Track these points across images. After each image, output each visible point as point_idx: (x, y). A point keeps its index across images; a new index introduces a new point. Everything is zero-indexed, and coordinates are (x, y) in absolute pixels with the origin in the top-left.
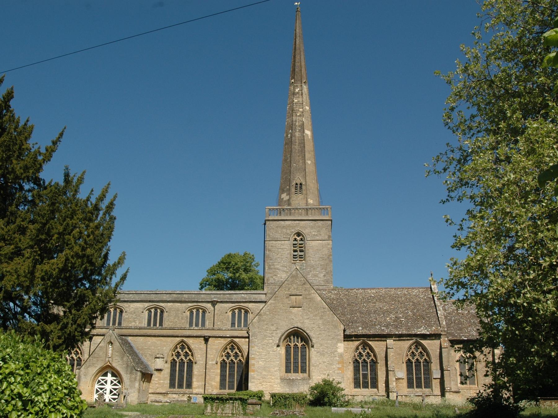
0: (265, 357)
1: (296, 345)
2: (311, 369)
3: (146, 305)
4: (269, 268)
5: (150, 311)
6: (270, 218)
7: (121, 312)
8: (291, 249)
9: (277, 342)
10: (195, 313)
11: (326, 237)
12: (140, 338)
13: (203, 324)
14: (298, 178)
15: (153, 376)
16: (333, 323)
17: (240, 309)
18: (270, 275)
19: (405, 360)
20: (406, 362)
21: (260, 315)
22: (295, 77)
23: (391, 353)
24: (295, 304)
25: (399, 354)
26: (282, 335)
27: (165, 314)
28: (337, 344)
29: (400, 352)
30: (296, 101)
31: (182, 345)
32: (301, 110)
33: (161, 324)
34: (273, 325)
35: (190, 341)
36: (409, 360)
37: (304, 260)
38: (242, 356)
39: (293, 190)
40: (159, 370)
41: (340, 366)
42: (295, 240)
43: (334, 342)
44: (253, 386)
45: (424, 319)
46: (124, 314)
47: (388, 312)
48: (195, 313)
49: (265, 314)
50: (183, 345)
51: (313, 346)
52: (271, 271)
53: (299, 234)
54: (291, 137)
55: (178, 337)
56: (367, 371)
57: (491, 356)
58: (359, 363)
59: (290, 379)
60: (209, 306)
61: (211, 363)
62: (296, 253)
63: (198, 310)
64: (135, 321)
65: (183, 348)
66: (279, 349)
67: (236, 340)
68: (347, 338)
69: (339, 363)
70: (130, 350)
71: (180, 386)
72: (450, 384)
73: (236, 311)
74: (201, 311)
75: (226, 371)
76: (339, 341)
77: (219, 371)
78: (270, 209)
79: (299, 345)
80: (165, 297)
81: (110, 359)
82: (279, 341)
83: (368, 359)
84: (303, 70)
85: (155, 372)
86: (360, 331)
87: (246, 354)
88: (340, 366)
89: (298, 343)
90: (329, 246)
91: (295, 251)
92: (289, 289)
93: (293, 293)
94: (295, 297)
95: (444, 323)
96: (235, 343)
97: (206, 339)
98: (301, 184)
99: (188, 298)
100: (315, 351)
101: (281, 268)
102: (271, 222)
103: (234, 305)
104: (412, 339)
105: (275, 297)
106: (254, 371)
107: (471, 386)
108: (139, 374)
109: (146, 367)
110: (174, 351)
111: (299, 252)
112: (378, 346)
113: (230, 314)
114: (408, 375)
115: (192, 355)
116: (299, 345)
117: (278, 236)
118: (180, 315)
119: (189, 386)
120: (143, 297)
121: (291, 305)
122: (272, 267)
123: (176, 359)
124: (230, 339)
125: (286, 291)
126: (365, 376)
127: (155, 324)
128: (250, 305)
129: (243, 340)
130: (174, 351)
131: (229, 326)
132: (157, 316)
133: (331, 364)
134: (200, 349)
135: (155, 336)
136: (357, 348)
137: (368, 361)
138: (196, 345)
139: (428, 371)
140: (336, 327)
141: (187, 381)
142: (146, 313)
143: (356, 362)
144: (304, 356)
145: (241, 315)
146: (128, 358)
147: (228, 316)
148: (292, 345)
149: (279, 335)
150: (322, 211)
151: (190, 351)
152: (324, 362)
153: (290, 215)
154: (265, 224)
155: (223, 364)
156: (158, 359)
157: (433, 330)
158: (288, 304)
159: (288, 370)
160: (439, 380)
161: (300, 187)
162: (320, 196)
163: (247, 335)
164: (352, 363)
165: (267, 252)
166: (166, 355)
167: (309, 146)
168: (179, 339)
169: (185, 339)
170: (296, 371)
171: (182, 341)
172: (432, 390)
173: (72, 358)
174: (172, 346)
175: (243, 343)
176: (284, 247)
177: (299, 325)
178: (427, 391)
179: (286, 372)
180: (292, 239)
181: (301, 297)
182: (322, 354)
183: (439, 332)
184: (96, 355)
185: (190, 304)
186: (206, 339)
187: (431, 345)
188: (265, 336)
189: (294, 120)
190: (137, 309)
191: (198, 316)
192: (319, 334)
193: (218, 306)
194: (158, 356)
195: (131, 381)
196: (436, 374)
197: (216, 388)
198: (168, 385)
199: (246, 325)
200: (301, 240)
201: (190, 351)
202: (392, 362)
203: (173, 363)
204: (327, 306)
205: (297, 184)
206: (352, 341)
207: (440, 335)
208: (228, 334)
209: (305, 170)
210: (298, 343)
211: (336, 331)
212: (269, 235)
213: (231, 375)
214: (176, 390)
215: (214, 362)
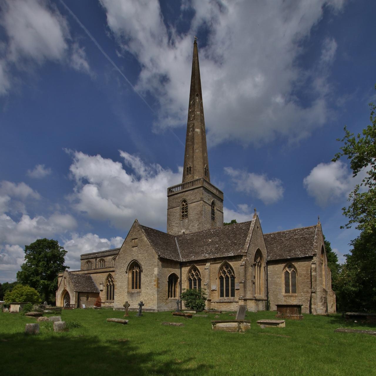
0: (121, 280)
1: (136, 271)
8: (180, 211)
11: (200, 199)
15: (100, 294)
34: (124, 260)
40: (102, 291)
57: (106, 258)
59: (131, 293)
85: (100, 292)
93: (134, 238)
100: (143, 274)
105: (126, 242)
107: (293, 294)
121: (132, 246)
133: (151, 282)
136: (221, 268)
152: (147, 281)
158: (132, 245)
166: (104, 282)
168: (108, 273)
169: (111, 273)
181: (137, 240)
182: (147, 276)
188: (121, 267)
194: (101, 283)
205: (188, 168)
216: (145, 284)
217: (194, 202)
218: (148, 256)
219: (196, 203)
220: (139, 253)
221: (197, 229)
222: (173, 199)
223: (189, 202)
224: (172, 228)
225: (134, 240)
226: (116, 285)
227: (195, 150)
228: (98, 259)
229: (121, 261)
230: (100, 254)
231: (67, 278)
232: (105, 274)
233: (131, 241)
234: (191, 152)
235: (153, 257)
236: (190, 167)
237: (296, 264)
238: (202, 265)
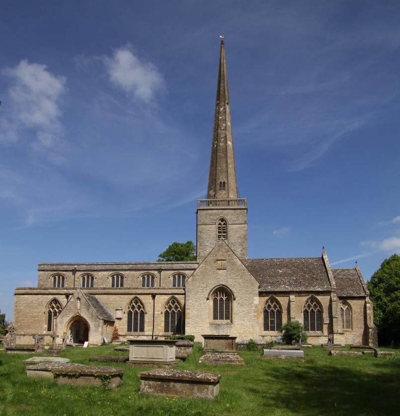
1: (221, 298)
2: (233, 316)
4: (201, 245)
5: (114, 278)
6: (201, 208)
7: (93, 278)
9: (207, 296)
10: (146, 278)
11: (243, 222)
12: (104, 295)
13: (153, 285)
14: (222, 179)
15: (115, 323)
16: (251, 282)
17: (179, 275)
18: (201, 250)
19: (303, 310)
20: (304, 312)
21: (194, 276)
22: (220, 98)
23: (293, 305)
24: (221, 267)
25: (298, 306)
26: (211, 291)
27: (125, 279)
28: (253, 297)
29: (300, 304)
30: (220, 118)
31: (136, 300)
32: (224, 125)
34: (203, 283)
35: (141, 297)
36: (306, 310)
37: (227, 239)
38: (181, 308)
39: (218, 187)
40: (119, 319)
41: (256, 314)
42: (220, 224)
44: (189, 331)
46: (94, 280)
48: (146, 278)
50: (137, 300)
51: (234, 299)
52: (202, 247)
53: (222, 220)
54: (217, 146)
55: (132, 294)
56: (274, 318)
58: (268, 312)
60: (156, 273)
61: (157, 313)
62: (220, 234)
63: (148, 277)
65: (136, 303)
66: (208, 301)
67: (176, 296)
68: (261, 294)
69: (255, 312)
70: (97, 304)
71: (136, 330)
72: (337, 328)
73: (177, 276)
74: (150, 276)
75: (169, 319)
76: (255, 295)
77: (163, 319)
78: (201, 201)
79: (224, 298)
80: (124, 267)
81: (79, 311)
83: (275, 309)
84: (225, 65)
85: (116, 321)
86: (269, 288)
87: (183, 305)
88: (256, 314)
89: (223, 300)
90: (245, 229)
91: (219, 232)
92: (216, 256)
93: (220, 258)
94: (220, 262)
95: (334, 283)
96: (175, 298)
97: (154, 296)
98: (224, 183)
101: (209, 245)
102: (202, 211)
103: (174, 272)
104: (308, 295)
106: (189, 318)
107: (348, 329)
108: (102, 321)
109: (110, 316)
110: (130, 305)
111: (223, 232)
112: (283, 300)
113: (172, 278)
114: (304, 321)
115: (144, 308)
116: (224, 298)
117: (208, 221)
118: (135, 280)
119: (142, 330)
121: (218, 268)
123: (132, 310)
124: (171, 296)
125: (213, 257)
126: (272, 322)
127: (117, 286)
128: (187, 272)
129: (181, 296)
130: (130, 305)
131: (171, 286)
132: (118, 279)
134: (149, 303)
135: (115, 294)
136: (267, 302)
137: (275, 311)
138: (147, 300)
139: (321, 318)
140: (252, 284)
141: (140, 326)
142: (111, 279)
143: (266, 312)
144: (228, 307)
145: (180, 279)
146: (93, 310)
147: (171, 280)
148: (219, 298)
149: (209, 291)
150: (239, 201)
152: (244, 311)
153: (216, 205)
154: (197, 213)
155: (167, 314)
156: (118, 311)
157: (325, 288)
159: (215, 318)
160: (327, 325)
161: (223, 185)
162: (238, 193)
163: (183, 292)
164: (263, 312)
165: (199, 233)
166: (124, 308)
167: (230, 154)
168: (133, 296)
170: (222, 318)
171: (136, 297)
172: (323, 332)
173: (55, 311)
174: (128, 301)
175: (180, 298)
176: (211, 229)
177: (224, 283)
178: (319, 333)
179: (214, 319)
180: (217, 223)
181: (225, 262)
182: (242, 305)
183: (331, 290)
184: (68, 308)
185: (142, 272)
186: (154, 296)
187: (324, 300)
189: (219, 133)
190: (104, 275)
191: (148, 279)
192: (240, 290)
193: (163, 273)
194: (118, 308)
195: (95, 327)
196: (326, 320)
197: (162, 331)
198: (127, 329)
199: (184, 285)
200: (224, 224)
202: (294, 312)
203: (130, 313)
204: (246, 269)
205: (221, 183)
206: (264, 296)
207: (331, 291)
208: (170, 291)
209: (227, 172)
210: (223, 300)
211: (253, 287)
212: (200, 221)
213: (173, 322)
214: (133, 332)
215: (160, 313)
216: (240, 314)
217: (237, 224)
219: (239, 225)
220: (229, 277)
221: (240, 254)
222: (206, 215)
223: (229, 222)
224: (204, 248)
225: (219, 262)
227: (229, 164)
228: (78, 274)
229: (198, 284)
230: (85, 266)
231: (83, 300)
232: (126, 296)
233: (215, 262)
234: (224, 165)
235: (252, 284)
236: (224, 183)
237: (352, 302)
238: (282, 296)
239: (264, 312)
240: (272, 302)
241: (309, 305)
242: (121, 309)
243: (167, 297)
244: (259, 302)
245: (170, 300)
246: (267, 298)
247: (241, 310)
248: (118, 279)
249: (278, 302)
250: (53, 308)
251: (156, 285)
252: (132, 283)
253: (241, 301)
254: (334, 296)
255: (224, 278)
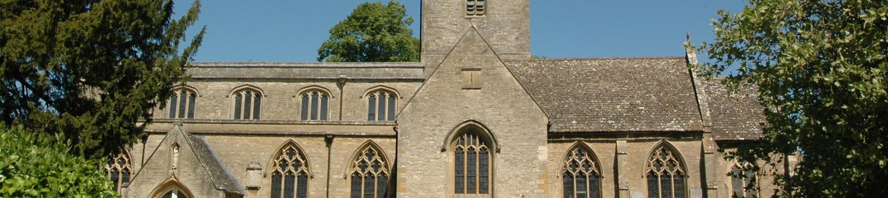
2: (495, 187)
3: (233, 85)
4: (429, 27)
5: (240, 96)
7: (193, 96)
9: (442, 144)
12: (223, 137)
13: (324, 116)
16: (532, 114)
17: (382, 92)
18: (430, 38)
19: (646, 172)
20: (648, 176)
21: (415, 101)
24: (470, 83)
26: (450, 133)
29: (638, 160)
31: (291, 148)
33: (256, 116)
34: (434, 117)
35: (302, 143)
36: (652, 172)
38: (386, 166)
40: (254, 189)
41: (542, 182)
43: (533, 143)
45: (676, 107)
46: (197, 100)
47: (619, 96)
49: (423, 99)
50: (292, 149)
51: (498, 151)
52: (432, 31)
55: (283, 135)
58: (572, 177)
60: (333, 86)
61: (336, 177)
63: (315, 94)
64: (214, 111)
65: (291, 154)
66: (444, 154)
67: (377, 141)
68: (554, 137)
70: (207, 156)
73: (377, 95)
76: (540, 143)
79: (477, 148)
80: (263, 73)
82: (445, 143)
85: (248, 192)
86: (574, 126)
87: (393, 163)
88: (542, 182)
92: (460, 60)
93: (467, 66)
94: (469, 72)
96: (374, 145)
97: (329, 140)
99: (300, 75)
100: (502, 158)
103: (372, 85)
106: (404, 190)
113: (366, 99)
115: (306, 165)
116: (477, 148)
118: (287, 101)
120: (227, 73)
121: (464, 85)
122: (434, 24)
123: (280, 171)
124: (366, 140)
125: (455, 63)
127: (247, 116)
128: (399, 86)
129: (388, 140)
130: (278, 159)
131: (365, 119)
132: (250, 103)
133: (528, 180)
134: (320, 155)
135: (247, 135)
136: (569, 154)
137: (587, 174)
138: (313, 148)
140: (535, 120)
142: (233, 98)
143: (567, 175)
144: (484, 167)
145: (384, 101)
146: (204, 170)
147: (364, 103)
148: (465, 148)
149: (445, 133)
151: (303, 158)
152: (517, 176)
155: (356, 179)
157: (690, 124)
163: (394, 133)
164: (561, 177)
166: (264, 165)
168: (285, 140)
171: (291, 143)
173: (115, 169)
174: (274, 150)
177: (477, 117)
182: (514, 163)
185: (303, 84)
186: (329, 140)
187: (687, 149)
188: (423, 134)
190: (219, 91)
191: (315, 102)
193: (347, 87)
194: (251, 166)
199: (392, 116)
201: (303, 158)
202: (625, 176)
203: (276, 177)
204: (521, 88)
206: (562, 142)
208: (364, 131)
211: (536, 126)
215: (341, 176)
218: (515, 115)
224: (437, 32)
226: (404, 180)
239: (564, 177)
240: (580, 154)
241: (658, 161)
242: (257, 166)
243: (356, 144)
244: (550, 157)
245: (364, 148)
246: (569, 146)
247: (511, 174)
248: (250, 103)
249: (677, 155)
250: (574, 164)
251: (331, 115)
252: (281, 109)
253: (512, 155)
254: (708, 141)
255: (478, 108)
